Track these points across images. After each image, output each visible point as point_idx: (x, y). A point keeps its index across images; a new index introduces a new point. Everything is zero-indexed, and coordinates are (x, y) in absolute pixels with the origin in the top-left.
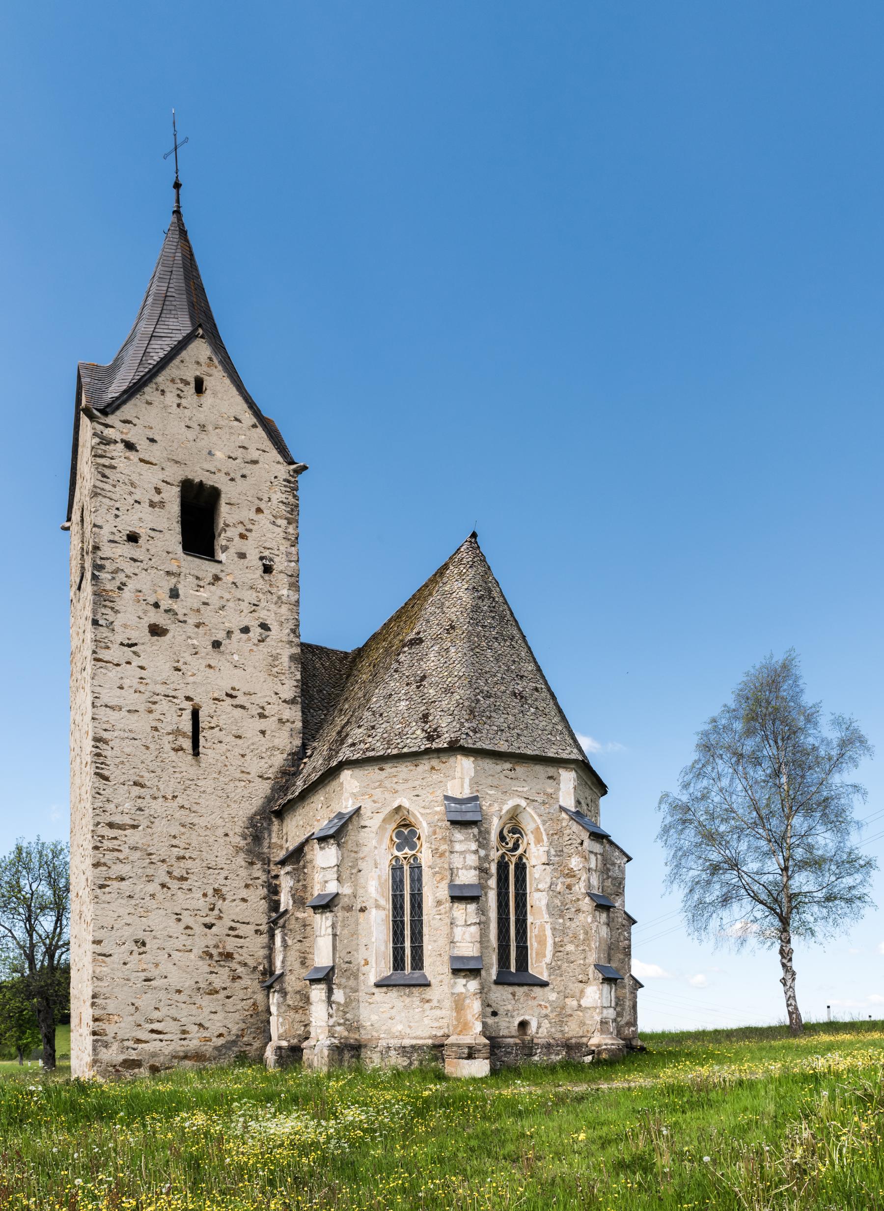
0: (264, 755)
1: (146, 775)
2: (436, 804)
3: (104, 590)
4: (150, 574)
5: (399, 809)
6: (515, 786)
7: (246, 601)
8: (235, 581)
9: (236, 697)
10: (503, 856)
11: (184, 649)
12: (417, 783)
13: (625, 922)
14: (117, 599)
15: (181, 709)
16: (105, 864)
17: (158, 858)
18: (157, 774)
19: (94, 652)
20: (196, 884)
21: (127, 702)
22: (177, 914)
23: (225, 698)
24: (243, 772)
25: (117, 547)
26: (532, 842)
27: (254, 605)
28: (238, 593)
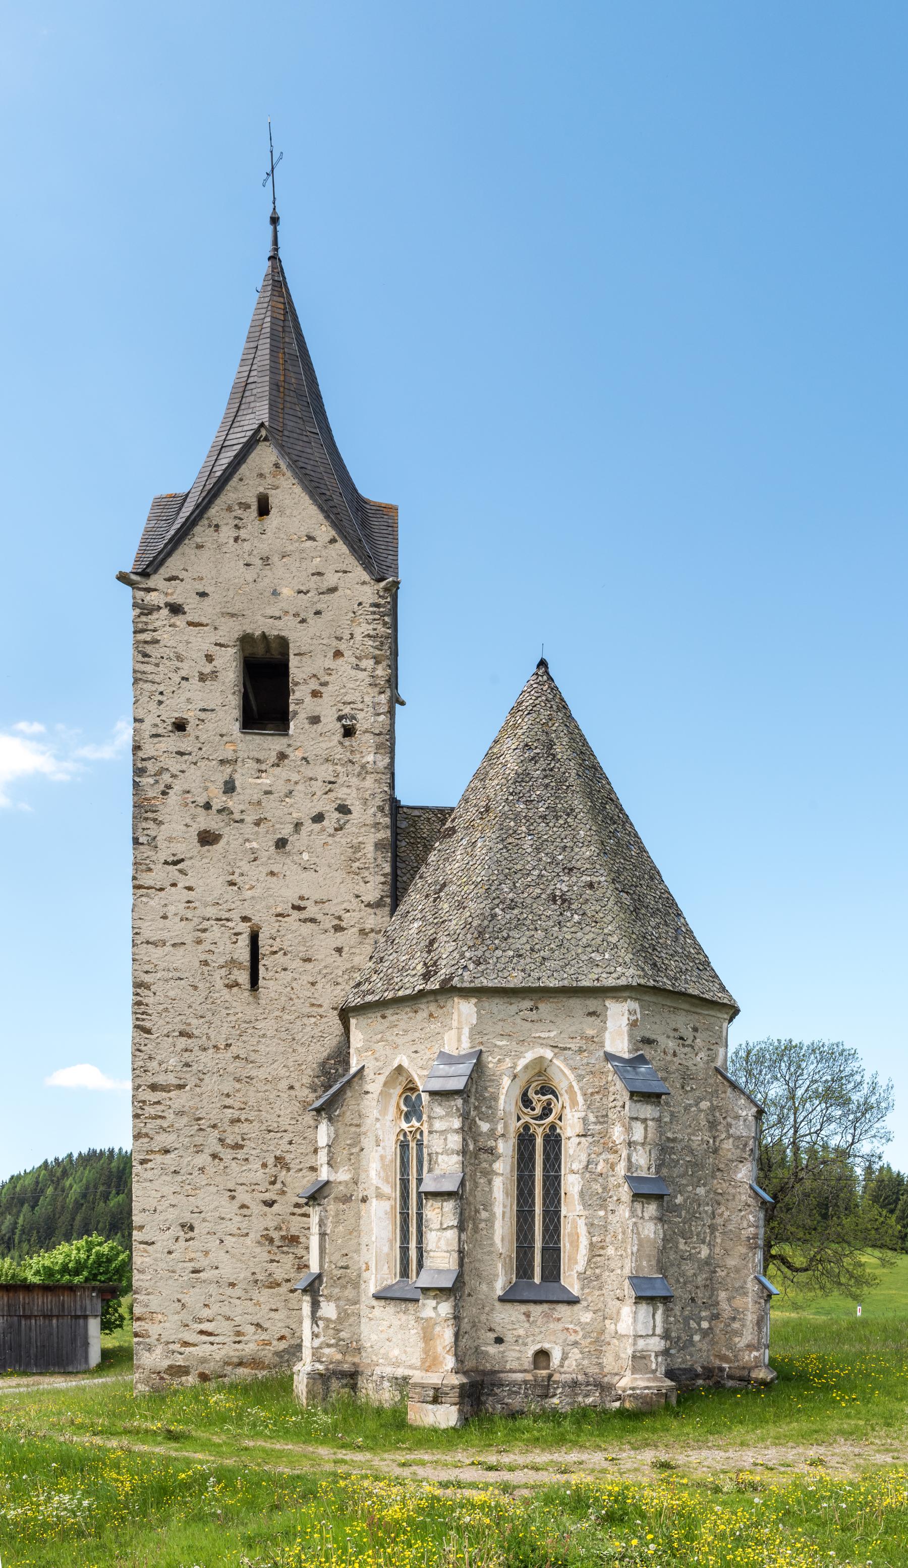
0: (340, 980)
1: (194, 1022)
3: (145, 799)
4: (199, 768)
5: (400, 1069)
6: (537, 1031)
7: (320, 780)
8: (306, 755)
9: (305, 908)
10: (526, 1127)
11: (240, 856)
12: (417, 1035)
14: (161, 808)
15: (236, 934)
16: (147, 1135)
17: (208, 1123)
18: (207, 1019)
19: (134, 878)
20: (254, 1152)
21: (172, 934)
22: (230, 1191)
23: (291, 911)
24: (313, 1005)
25: (160, 742)
26: (567, 1104)
27: (330, 783)
28: (309, 772)
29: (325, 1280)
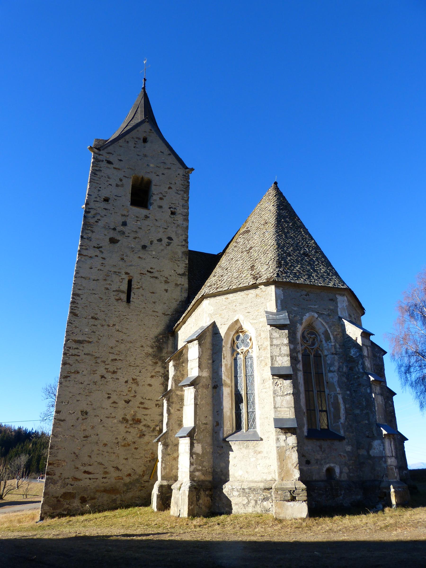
2: (260, 317)
13: (388, 394)
22: (109, 394)
27: (165, 229)
29: (197, 430)
